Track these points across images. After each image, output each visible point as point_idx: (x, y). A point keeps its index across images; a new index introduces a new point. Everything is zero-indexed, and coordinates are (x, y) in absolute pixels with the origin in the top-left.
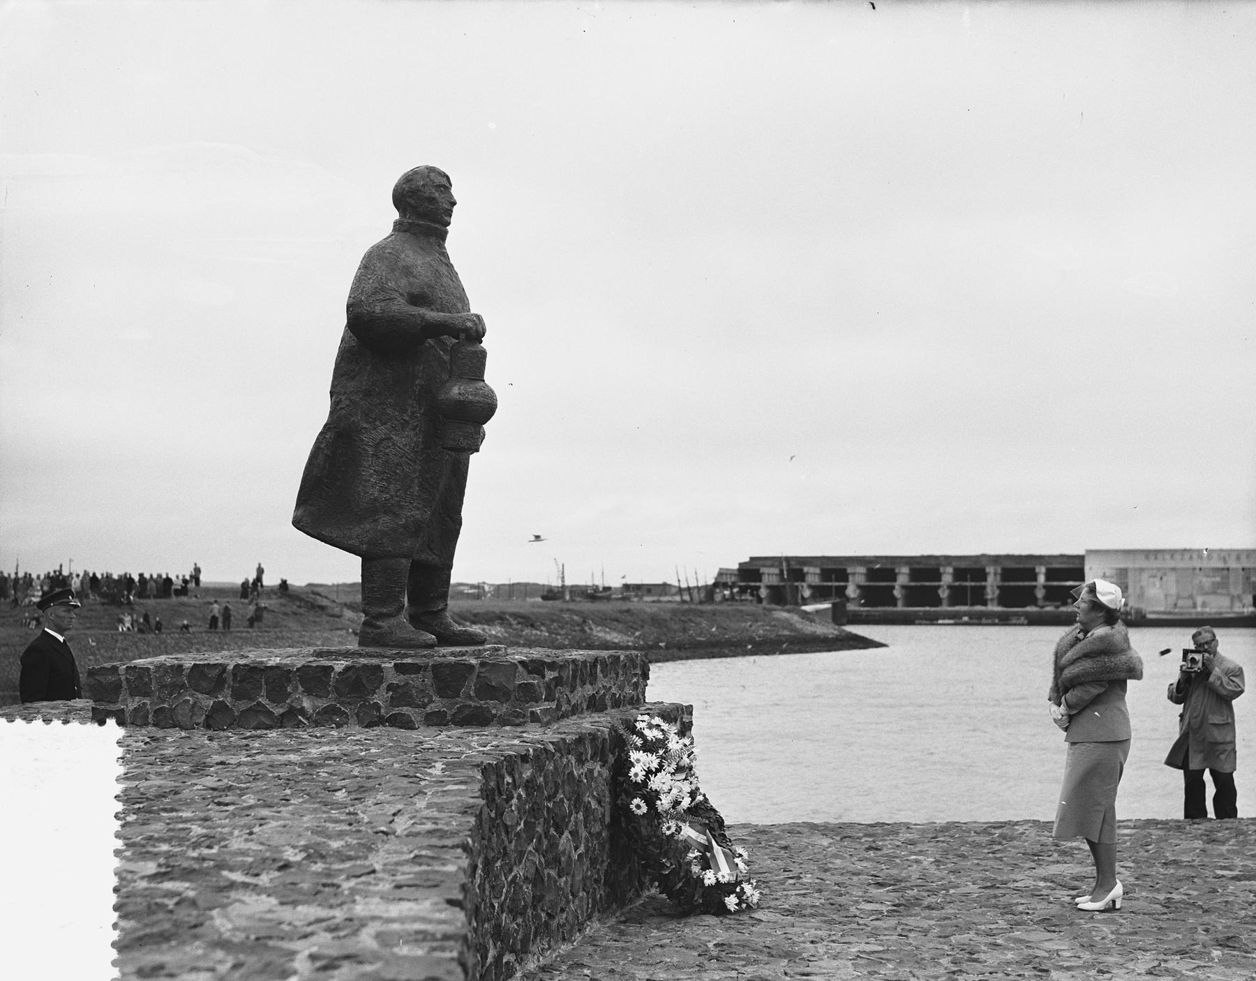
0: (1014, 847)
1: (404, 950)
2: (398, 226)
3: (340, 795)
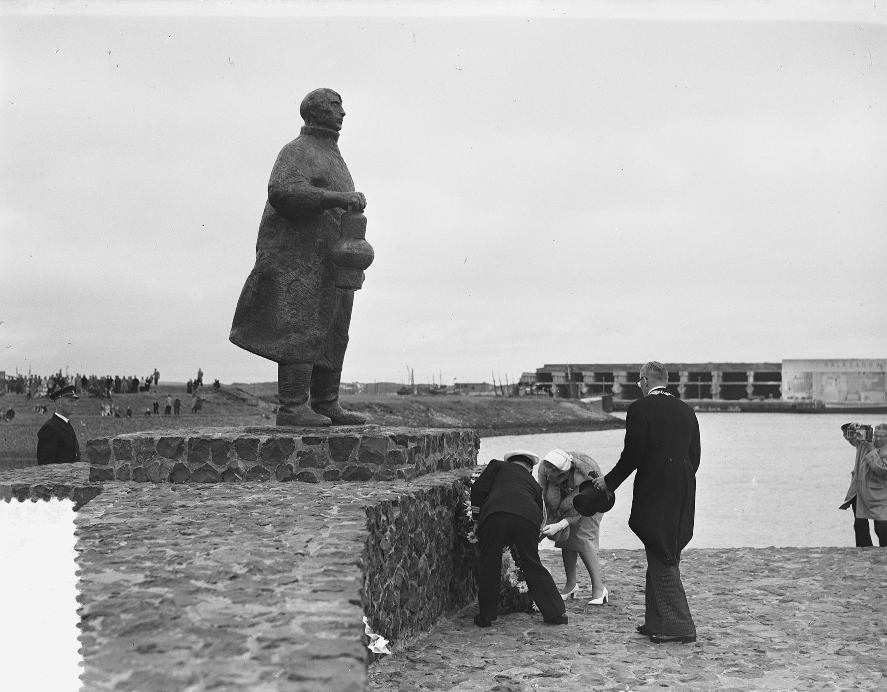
0: (737, 566)
1: (323, 635)
2: (304, 131)
3: (269, 528)
